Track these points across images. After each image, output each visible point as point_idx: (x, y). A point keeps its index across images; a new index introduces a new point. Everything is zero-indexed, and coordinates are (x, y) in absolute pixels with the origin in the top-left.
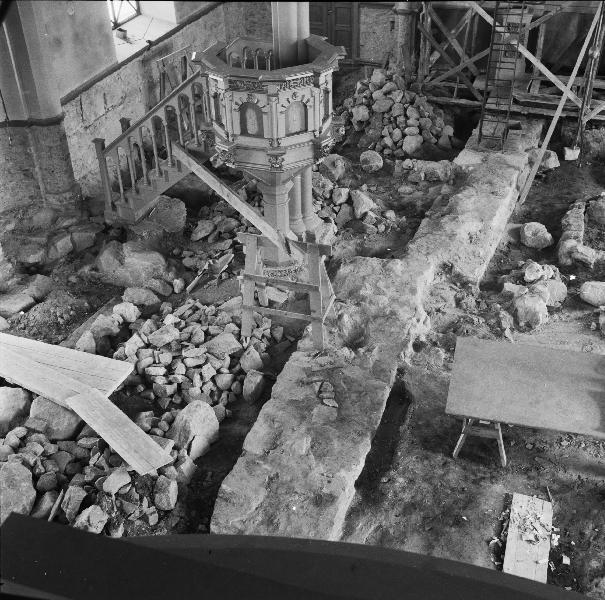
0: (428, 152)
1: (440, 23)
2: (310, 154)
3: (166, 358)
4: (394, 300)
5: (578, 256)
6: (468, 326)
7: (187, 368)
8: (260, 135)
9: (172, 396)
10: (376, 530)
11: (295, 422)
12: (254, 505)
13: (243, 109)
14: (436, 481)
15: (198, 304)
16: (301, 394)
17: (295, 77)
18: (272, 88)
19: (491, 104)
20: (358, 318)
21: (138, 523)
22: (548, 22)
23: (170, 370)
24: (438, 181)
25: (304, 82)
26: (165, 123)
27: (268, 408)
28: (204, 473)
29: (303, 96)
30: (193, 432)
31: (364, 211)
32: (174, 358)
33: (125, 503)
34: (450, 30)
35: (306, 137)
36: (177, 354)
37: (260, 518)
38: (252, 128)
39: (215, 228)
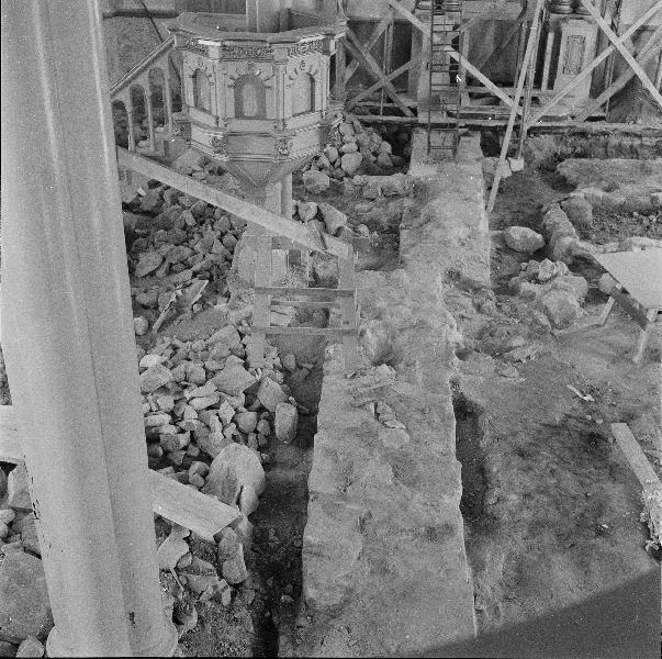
0: (367, 169)
1: (353, 38)
2: (316, 140)
3: (167, 402)
4: (415, 310)
5: (579, 252)
6: (505, 329)
7: (198, 412)
8: (261, 116)
9: (185, 448)
10: (508, 559)
11: (363, 451)
12: (355, 554)
13: (238, 85)
14: (553, 492)
15: (177, 343)
16: (357, 418)
17: (311, 39)
18: (279, 53)
19: (422, 118)
20: (381, 333)
21: (209, 604)
22: (472, 30)
23: (175, 418)
24: (396, 196)
25: (313, 47)
26: (129, 109)
27: (320, 440)
28: (264, 532)
29: (311, 66)
30: (241, 481)
31: (339, 225)
32: (175, 402)
33: (194, 578)
34: (362, 43)
35: (314, 118)
36: (178, 398)
37: (368, 568)
38: (250, 107)
39: (164, 260)
